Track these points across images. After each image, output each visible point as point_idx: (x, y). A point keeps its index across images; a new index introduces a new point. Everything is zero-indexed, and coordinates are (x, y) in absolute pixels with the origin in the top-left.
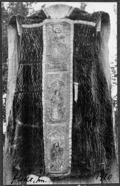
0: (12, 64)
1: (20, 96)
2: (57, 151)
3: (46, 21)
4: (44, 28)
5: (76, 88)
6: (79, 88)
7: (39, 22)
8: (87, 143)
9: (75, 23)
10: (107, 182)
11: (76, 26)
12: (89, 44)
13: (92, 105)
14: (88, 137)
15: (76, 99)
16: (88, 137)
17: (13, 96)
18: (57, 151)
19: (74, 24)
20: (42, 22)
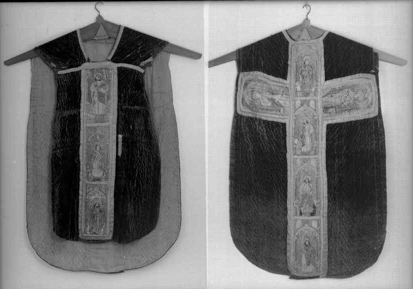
0: (58, 83)
1: (59, 153)
2: (96, 212)
3: (85, 65)
4: (83, 74)
5: (120, 140)
6: (123, 139)
7: (77, 66)
8: (129, 205)
9: (119, 66)
10: (3, 64)
11: (119, 69)
12: (135, 91)
13: (137, 162)
14: (131, 198)
15: (120, 154)
16: (131, 198)
17: (56, 235)
18: (96, 212)
19: (118, 68)
20: (80, 65)
